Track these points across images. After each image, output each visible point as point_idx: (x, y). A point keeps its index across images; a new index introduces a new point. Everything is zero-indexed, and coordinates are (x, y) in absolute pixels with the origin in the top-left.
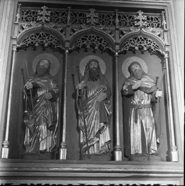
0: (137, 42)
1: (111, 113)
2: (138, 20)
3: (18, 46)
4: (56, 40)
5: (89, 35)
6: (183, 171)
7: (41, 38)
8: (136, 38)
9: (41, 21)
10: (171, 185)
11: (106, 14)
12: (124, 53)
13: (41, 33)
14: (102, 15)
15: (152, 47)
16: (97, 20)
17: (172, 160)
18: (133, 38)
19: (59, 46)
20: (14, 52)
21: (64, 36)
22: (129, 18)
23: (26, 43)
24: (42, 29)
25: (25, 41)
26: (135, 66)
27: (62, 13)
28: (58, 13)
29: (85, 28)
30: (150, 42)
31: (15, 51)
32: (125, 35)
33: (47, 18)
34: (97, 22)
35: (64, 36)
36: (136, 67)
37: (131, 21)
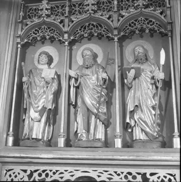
0: (41, 32)
1: (156, 102)
2: (42, 10)
3: (22, 43)
4: (105, 28)
5: (52, 28)
6: (179, 159)
7: (140, 25)
8: (40, 29)
9: (88, 10)
10: (104, 181)
11: (54, 5)
12: (163, 35)
13: (140, 19)
14: (102, 2)
15: (103, 32)
16: (49, 11)
17: (173, 147)
18: (48, 27)
19: (108, 35)
20: (19, 49)
21: (111, 23)
22: (62, 7)
23: (125, 32)
24: (141, 14)
25: (75, 35)
26: (138, 48)
27: (79, 5)
28: (57, 7)
29: (36, 20)
30: (92, 27)
31: (117, 41)
32: (74, 22)
33: (48, 11)
34: (96, 9)
35: (111, 23)
36: (140, 49)
37: (153, 2)
